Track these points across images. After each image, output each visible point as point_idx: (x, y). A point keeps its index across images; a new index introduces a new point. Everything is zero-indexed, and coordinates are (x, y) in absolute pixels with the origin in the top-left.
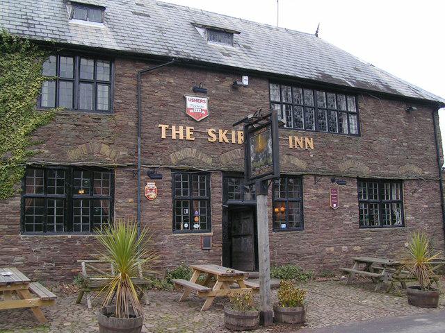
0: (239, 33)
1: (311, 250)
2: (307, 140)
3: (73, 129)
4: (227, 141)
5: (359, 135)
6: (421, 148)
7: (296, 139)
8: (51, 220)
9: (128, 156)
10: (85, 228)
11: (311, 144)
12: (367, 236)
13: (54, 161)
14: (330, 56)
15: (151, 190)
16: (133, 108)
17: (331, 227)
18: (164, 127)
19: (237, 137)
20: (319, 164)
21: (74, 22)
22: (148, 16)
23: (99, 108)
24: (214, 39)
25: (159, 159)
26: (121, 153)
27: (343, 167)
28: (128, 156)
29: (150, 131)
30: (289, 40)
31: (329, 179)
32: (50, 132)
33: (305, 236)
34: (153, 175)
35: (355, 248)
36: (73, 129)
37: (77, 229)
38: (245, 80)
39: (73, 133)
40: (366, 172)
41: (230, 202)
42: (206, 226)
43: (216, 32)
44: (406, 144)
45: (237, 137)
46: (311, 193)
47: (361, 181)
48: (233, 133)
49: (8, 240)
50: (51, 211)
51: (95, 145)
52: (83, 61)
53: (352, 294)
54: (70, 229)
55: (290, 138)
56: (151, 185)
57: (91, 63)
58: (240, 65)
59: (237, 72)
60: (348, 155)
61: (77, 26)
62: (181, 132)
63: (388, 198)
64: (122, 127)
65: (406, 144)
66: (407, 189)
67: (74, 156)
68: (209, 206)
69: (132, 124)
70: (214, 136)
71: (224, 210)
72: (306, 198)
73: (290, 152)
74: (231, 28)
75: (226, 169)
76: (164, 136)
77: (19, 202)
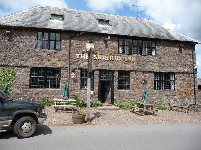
0: (111, 21)
1: (133, 97)
2: (133, 58)
3: (47, 56)
4: (101, 59)
5: (156, 56)
6: (185, 60)
7: (128, 58)
8: (40, 84)
9: (65, 64)
10: (51, 87)
11: (135, 59)
12: (157, 93)
13: (41, 66)
14: (151, 27)
15: (73, 75)
16: (68, 48)
17: (142, 89)
18: (78, 55)
19: (85, 56)
20: (137, 67)
21: (51, 21)
22: (81, 17)
23: (120, 53)
24: (102, 23)
25: (76, 65)
26: (63, 63)
27: (148, 68)
28: (65, 64)
29: (73, 56)
30: (135, 22)
31: (141, 74)
32: (40, 57)
33: (130, 92)
34: (74, 70)
35: (152, 97)
36: (47, 56)
37: (48, 87)
38: (109, 38)
39: (47, 57)
40: (157, 69)
41: (101, 80)
42: (92, 87)
43: (102, 21)
44: (177, 59)
45: (85, 56)
46: (133, 76)
47: (157, 74)
48: (103, 56)
49: (25, 90)
50: (40, 82)
51: (54, 61)
52: (51, 34)
53: (176, 116)
54: (46, 87)
55: (126, 58)
56: (73, 74)
57: (54, 34)
58: (107, 33)
59: (106, 35)
60: (150, 63)
61: (52, 22)
62: (84, 56)
63: (168, 79)
64: (64, 55)
65: (177, 59)
66: (177, 77)
67: (47, 64)
68: (94, 81)
69: (67, 54)
70: (96, 57)
71: (99, 83)
72: (131, 79)
73: (126, 63)
74: (108, 20)
75: (120, 69)
76: (78, 58)
77: (29, 78)
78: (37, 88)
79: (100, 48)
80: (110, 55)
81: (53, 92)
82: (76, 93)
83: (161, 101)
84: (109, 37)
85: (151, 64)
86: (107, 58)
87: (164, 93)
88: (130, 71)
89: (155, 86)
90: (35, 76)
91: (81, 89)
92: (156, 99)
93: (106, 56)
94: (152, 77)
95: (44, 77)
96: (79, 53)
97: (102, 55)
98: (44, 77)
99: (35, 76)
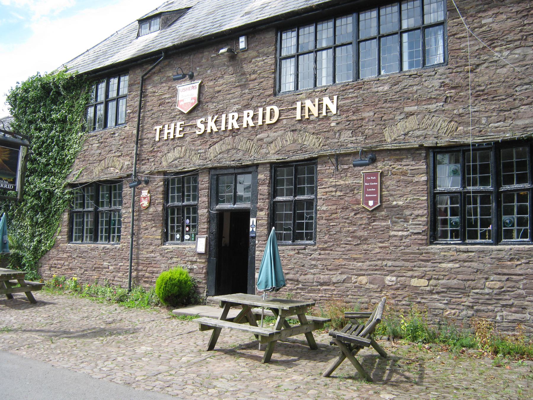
1: (323, 278)
12: (445, 259)
33: (315, 255)
35: (415, 282)
38: (242, 43)
60: (407, 109)
78: (463, 239)
79: (217, 89)
80: (247, 107)
81: (106, 251)
82: (152, 255)
83: (467, 301)
84: (242, 39)
85: (414, 108)
86: (233, 123)
87: (487, 259)
88: (312, 162)
89: (433, 224)
90: (482, 188)
91: (431, 243)
92: (439, 289)
93: (230, 115)
94: (416, 179)
95: (527, 185)
96: (161, 124)
97: (219, 112)
98: (527, 185)
99: (482, 188)
